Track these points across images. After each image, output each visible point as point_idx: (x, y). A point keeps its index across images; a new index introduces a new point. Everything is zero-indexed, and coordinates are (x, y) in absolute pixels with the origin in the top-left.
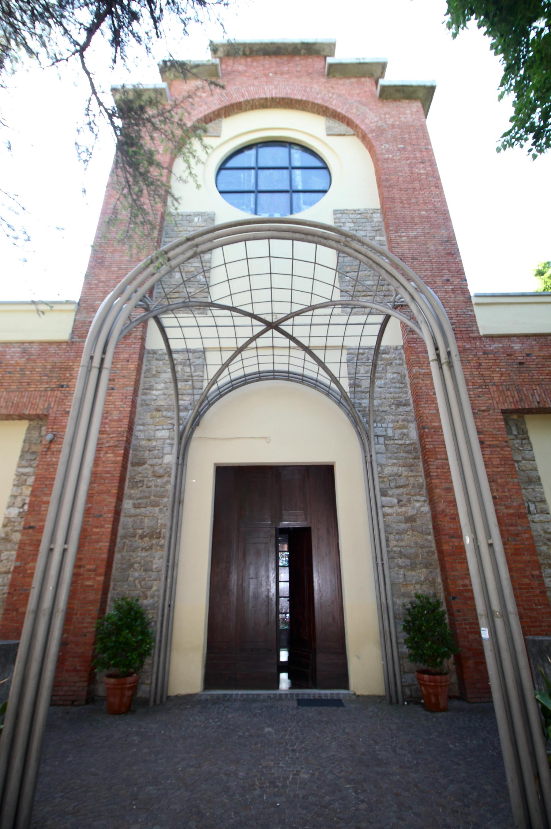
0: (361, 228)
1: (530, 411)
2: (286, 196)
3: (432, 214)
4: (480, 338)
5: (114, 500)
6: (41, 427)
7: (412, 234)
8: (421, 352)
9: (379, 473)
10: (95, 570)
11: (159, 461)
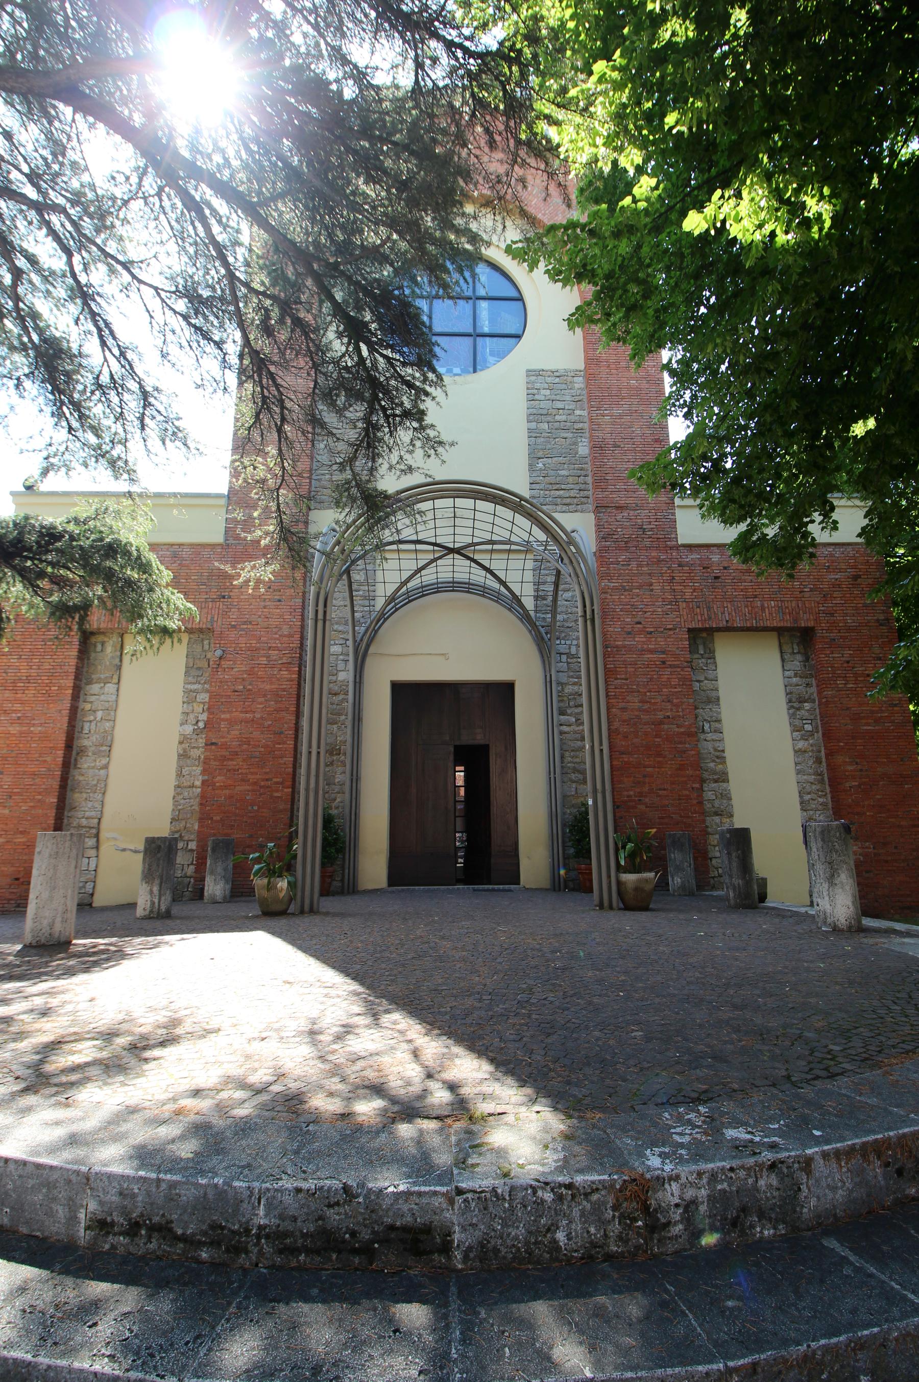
0: (558, 397)
1: (719, 630)
2: (468, 341)
3: (644, 385)
4: (678, 547)
5: (293, 718)
6: (203, 640)
7: (616, 412)
8: (612, 563)
9: (559, 692)
10: (282, 783)
11: (334, 678)
